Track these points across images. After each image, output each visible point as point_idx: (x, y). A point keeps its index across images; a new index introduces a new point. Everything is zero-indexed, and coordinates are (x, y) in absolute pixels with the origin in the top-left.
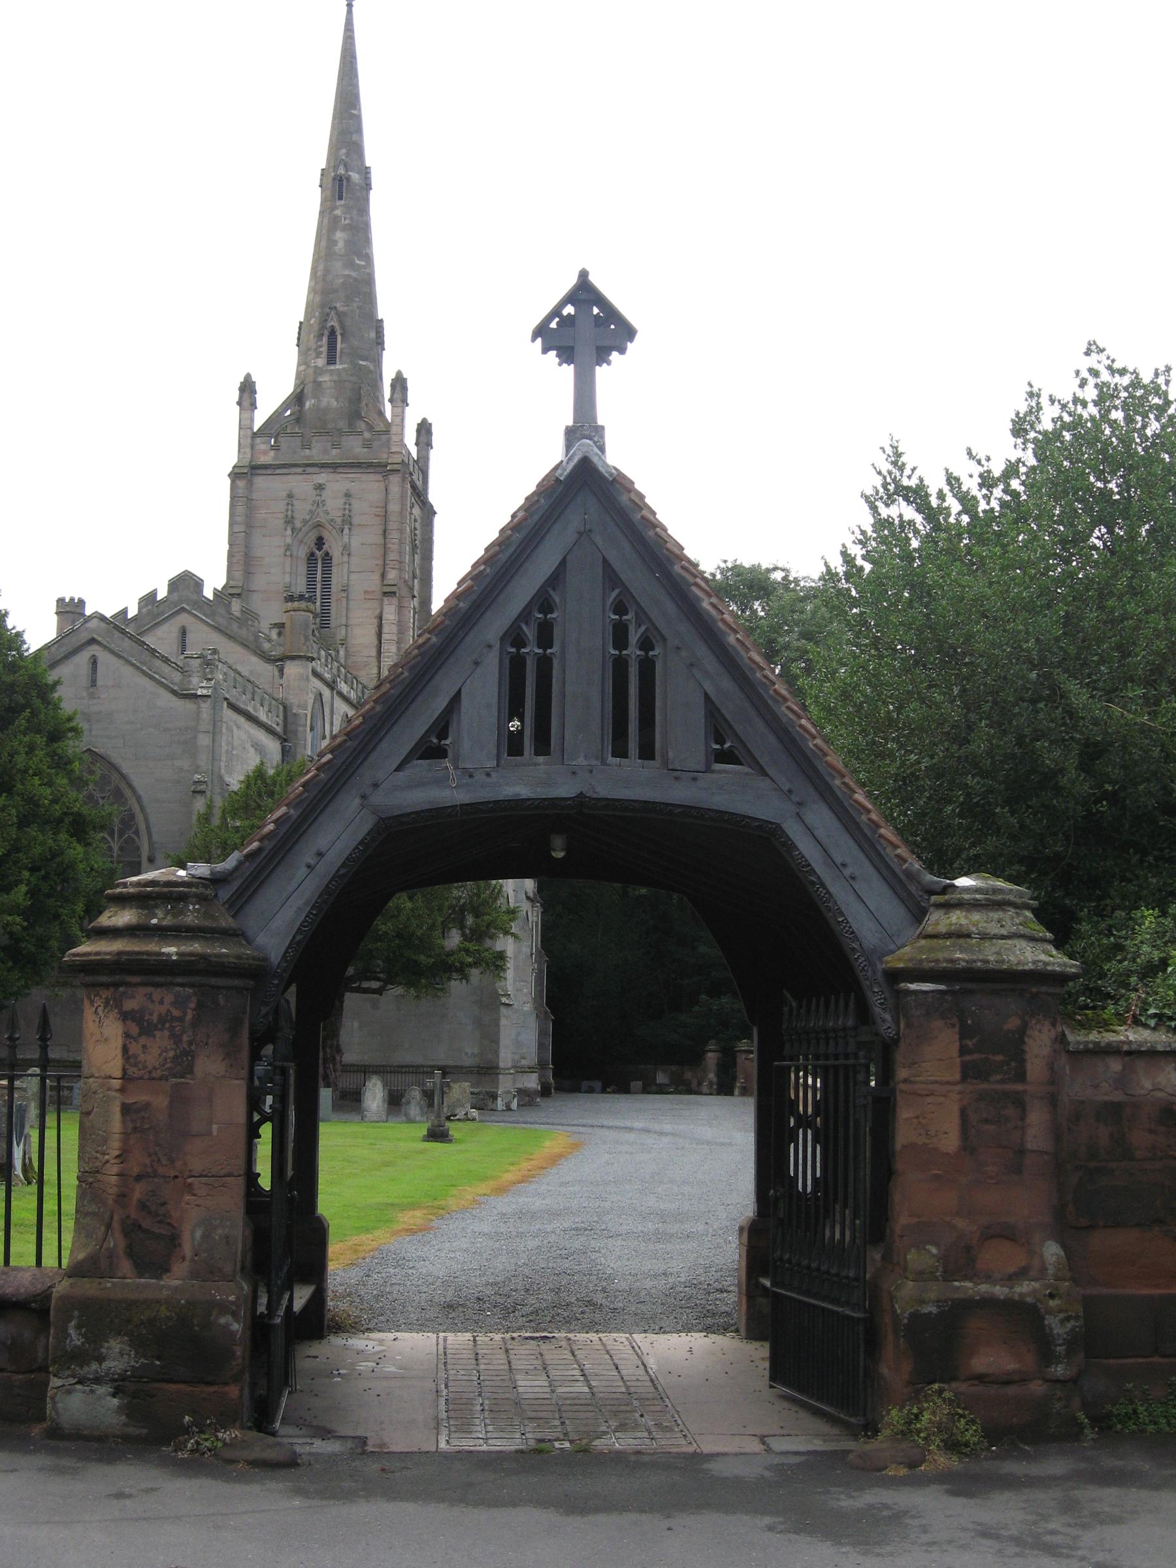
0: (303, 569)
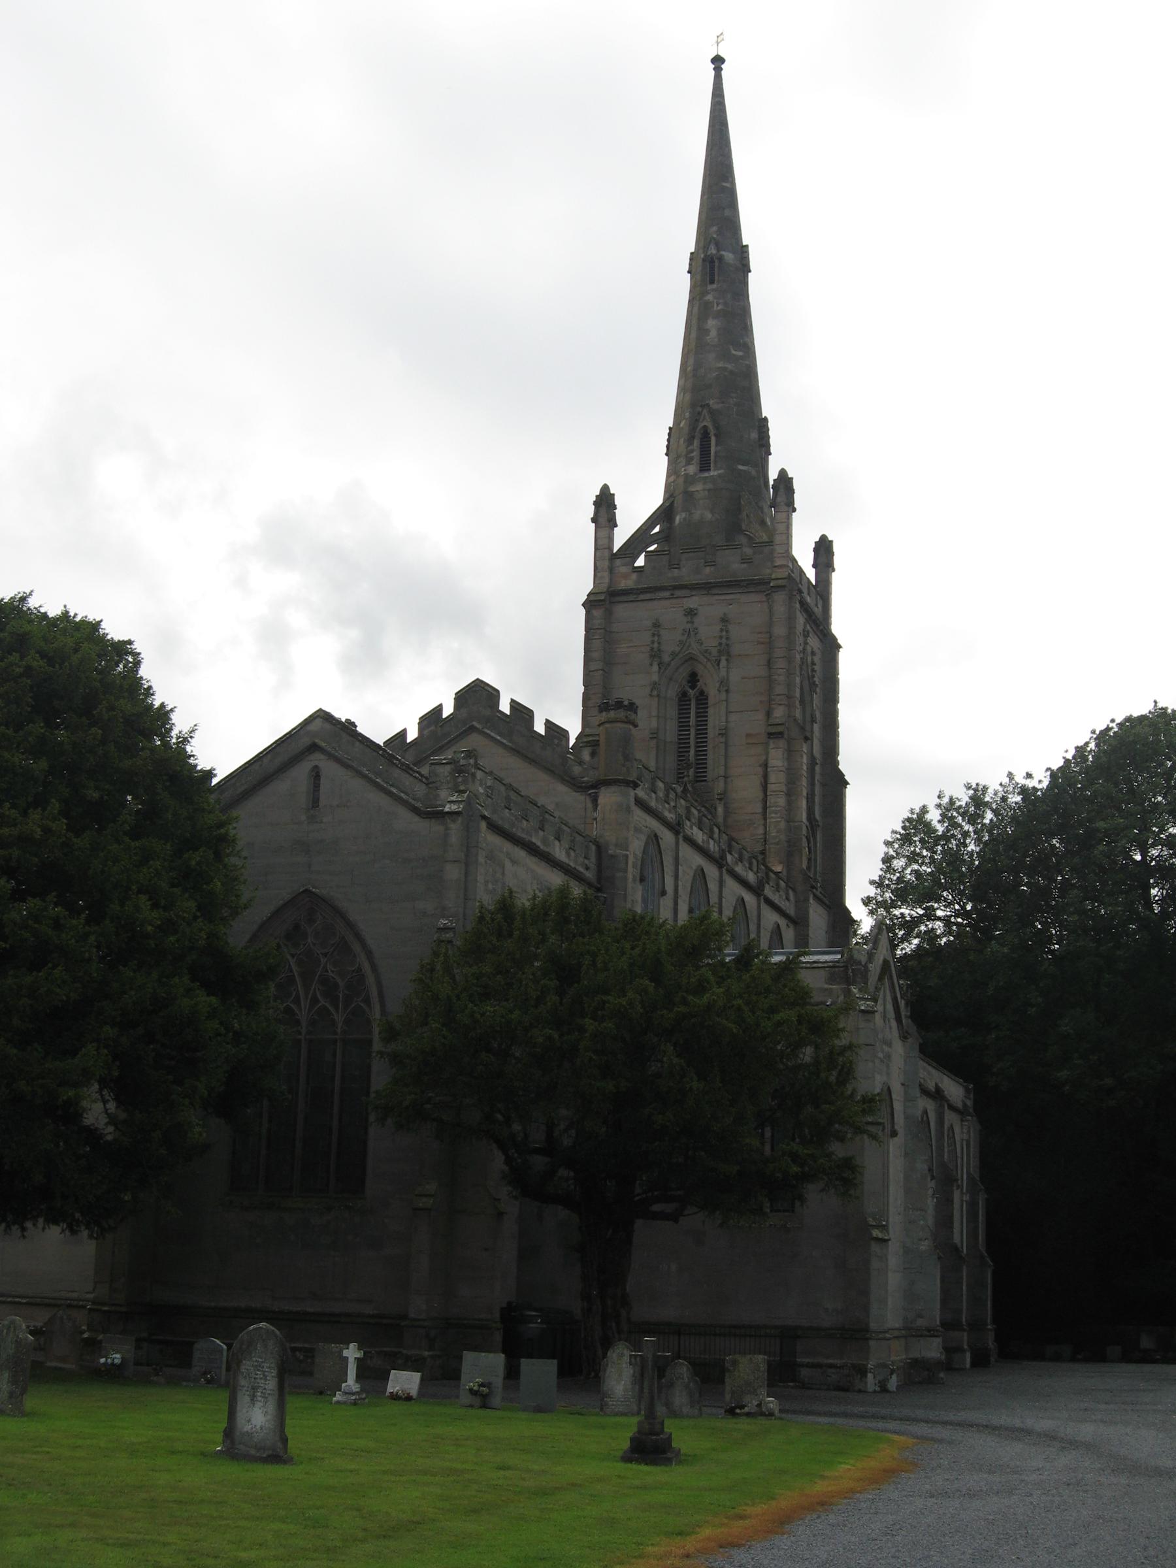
0: (672, 712)
